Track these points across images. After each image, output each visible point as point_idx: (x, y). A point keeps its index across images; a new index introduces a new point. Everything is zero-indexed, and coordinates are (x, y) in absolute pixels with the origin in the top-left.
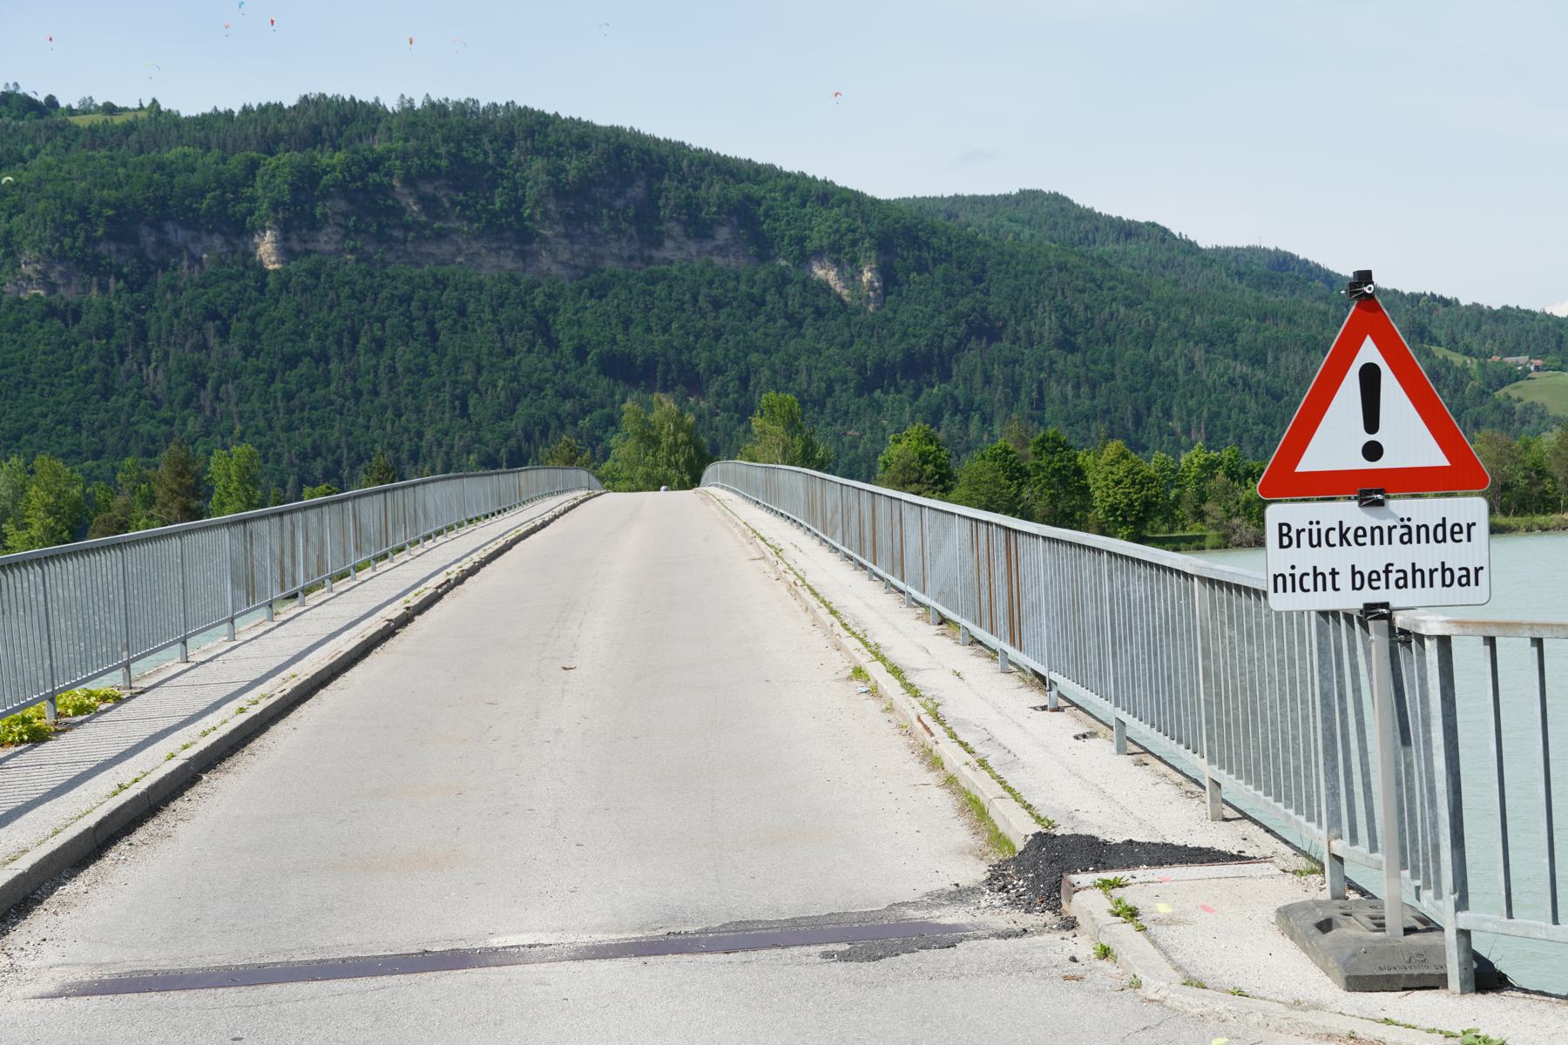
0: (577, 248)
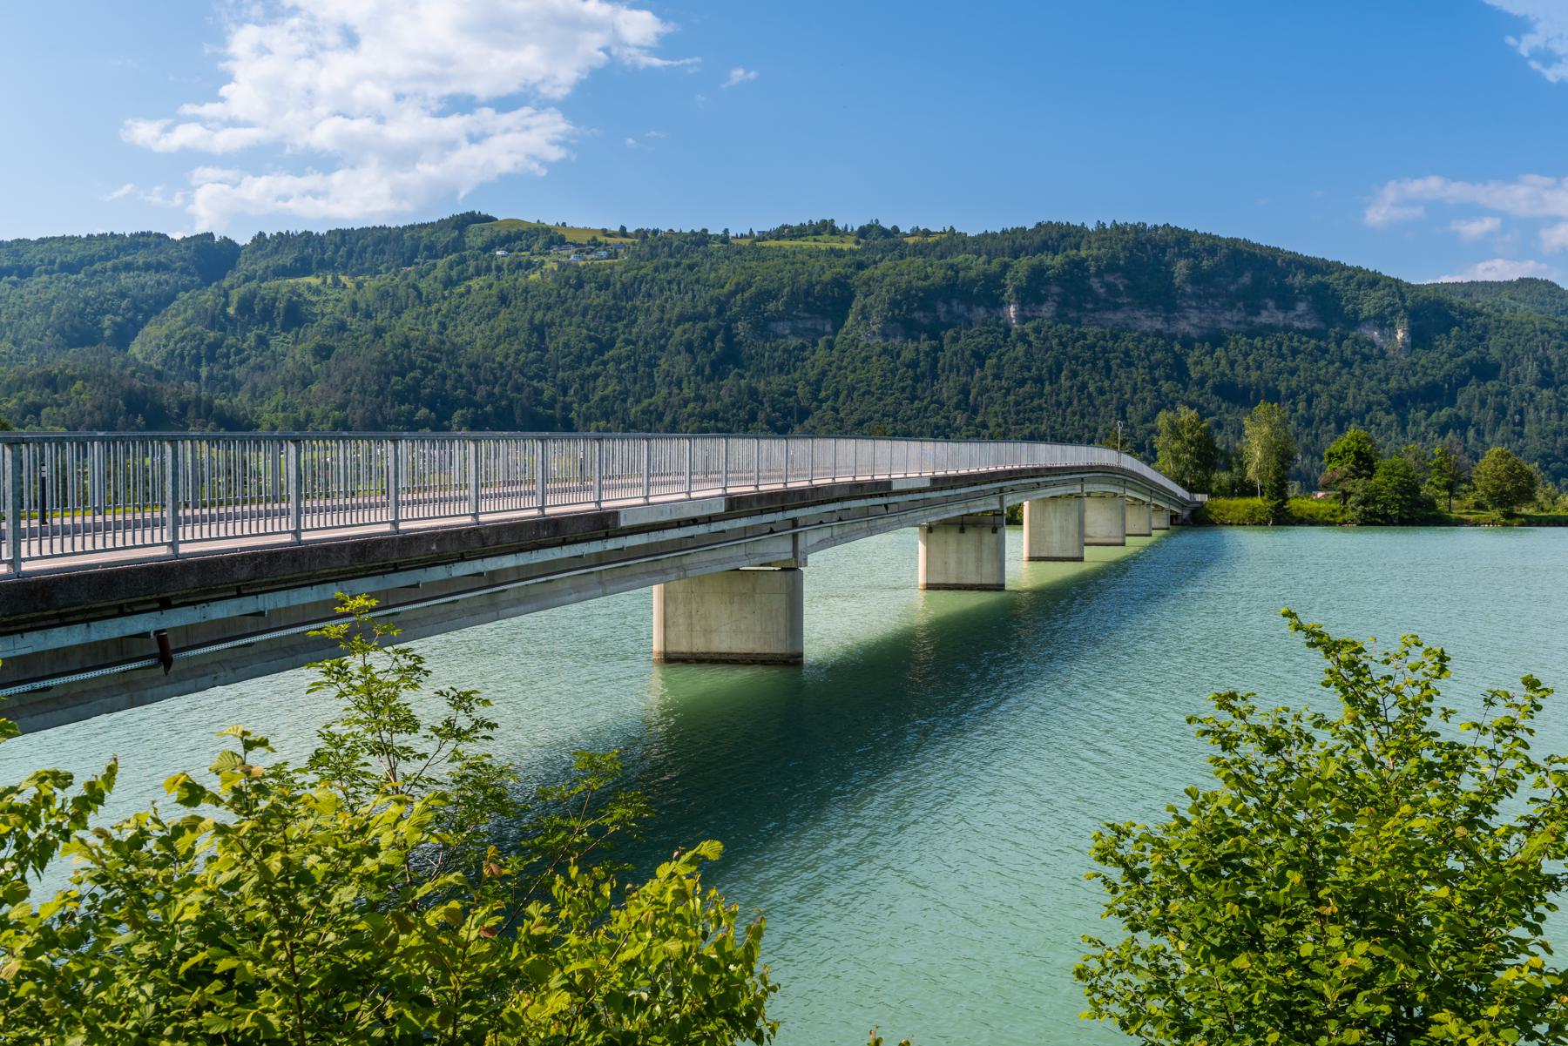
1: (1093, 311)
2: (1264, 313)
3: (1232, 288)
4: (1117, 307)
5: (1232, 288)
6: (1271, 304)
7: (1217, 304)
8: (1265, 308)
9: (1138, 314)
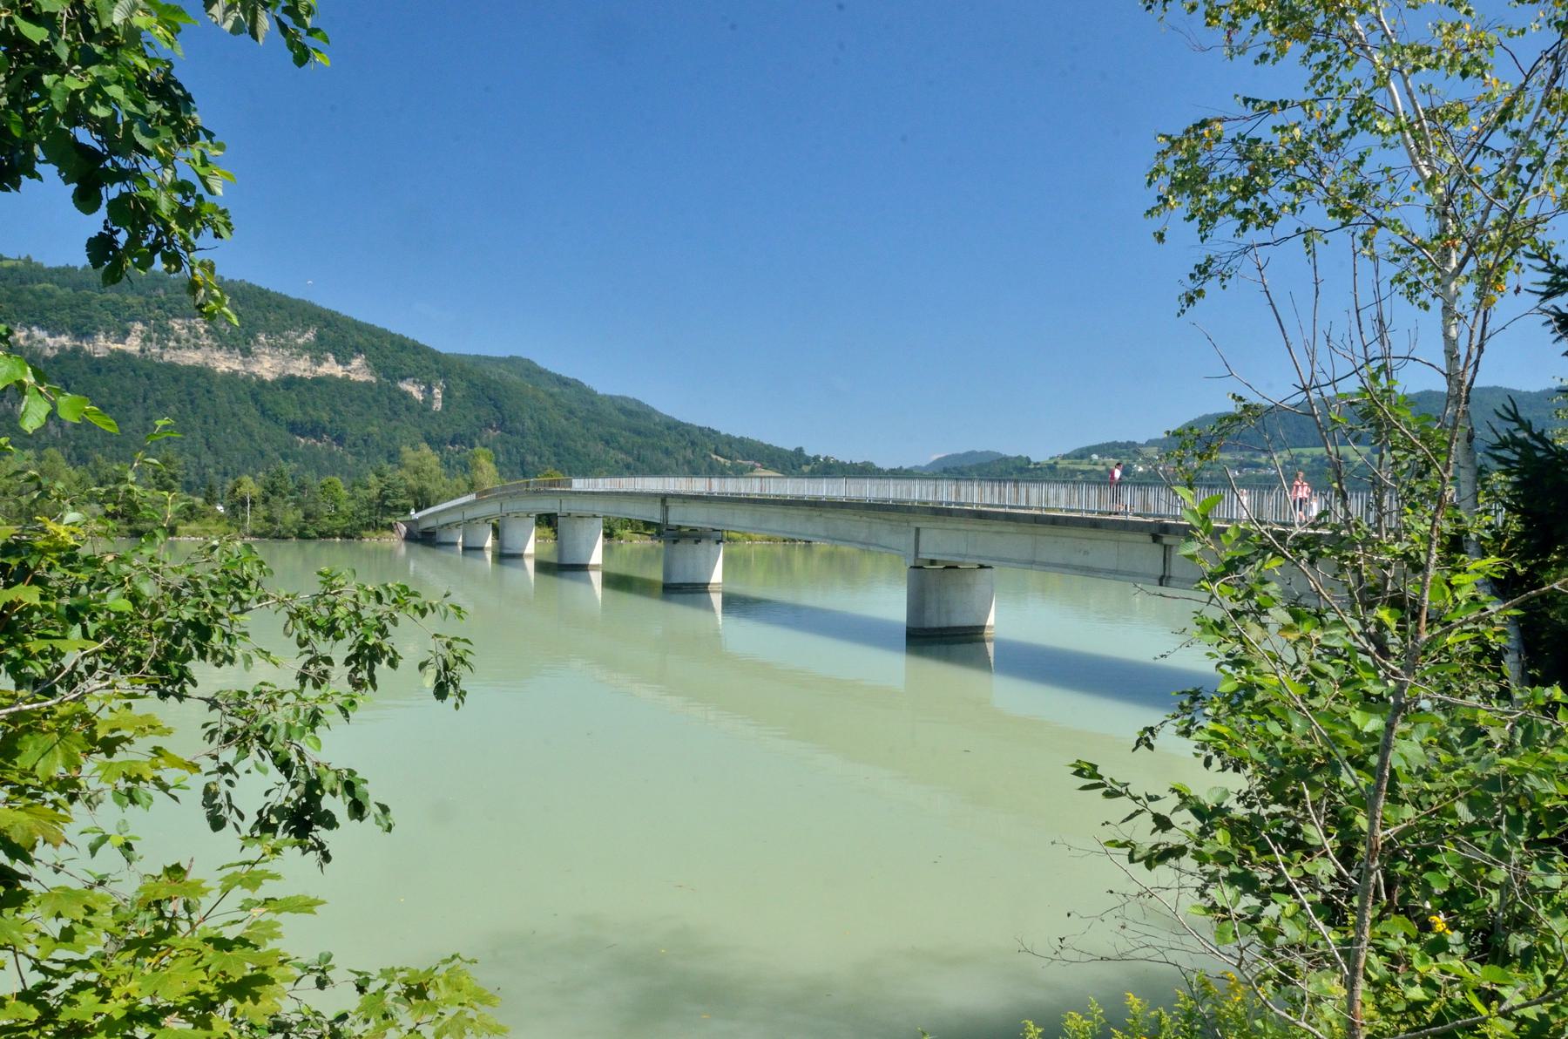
0: (275, 361)
1: (174, 348)
2: (326, 365)
3: (300, 341)
4: (197, 347)
5: (300, 341)
6: (331, 358)
7: (287, 353)
8: (327, 361)
9: (217, 355)
